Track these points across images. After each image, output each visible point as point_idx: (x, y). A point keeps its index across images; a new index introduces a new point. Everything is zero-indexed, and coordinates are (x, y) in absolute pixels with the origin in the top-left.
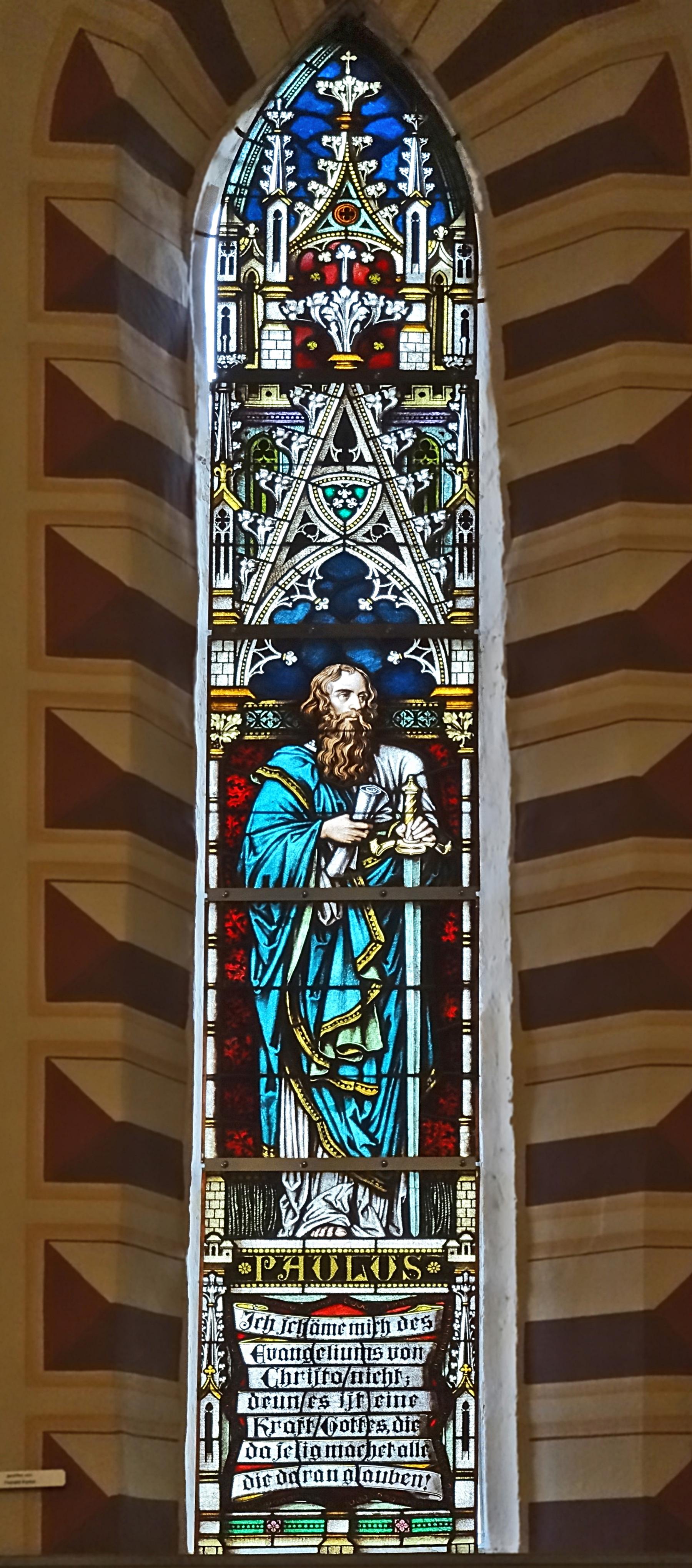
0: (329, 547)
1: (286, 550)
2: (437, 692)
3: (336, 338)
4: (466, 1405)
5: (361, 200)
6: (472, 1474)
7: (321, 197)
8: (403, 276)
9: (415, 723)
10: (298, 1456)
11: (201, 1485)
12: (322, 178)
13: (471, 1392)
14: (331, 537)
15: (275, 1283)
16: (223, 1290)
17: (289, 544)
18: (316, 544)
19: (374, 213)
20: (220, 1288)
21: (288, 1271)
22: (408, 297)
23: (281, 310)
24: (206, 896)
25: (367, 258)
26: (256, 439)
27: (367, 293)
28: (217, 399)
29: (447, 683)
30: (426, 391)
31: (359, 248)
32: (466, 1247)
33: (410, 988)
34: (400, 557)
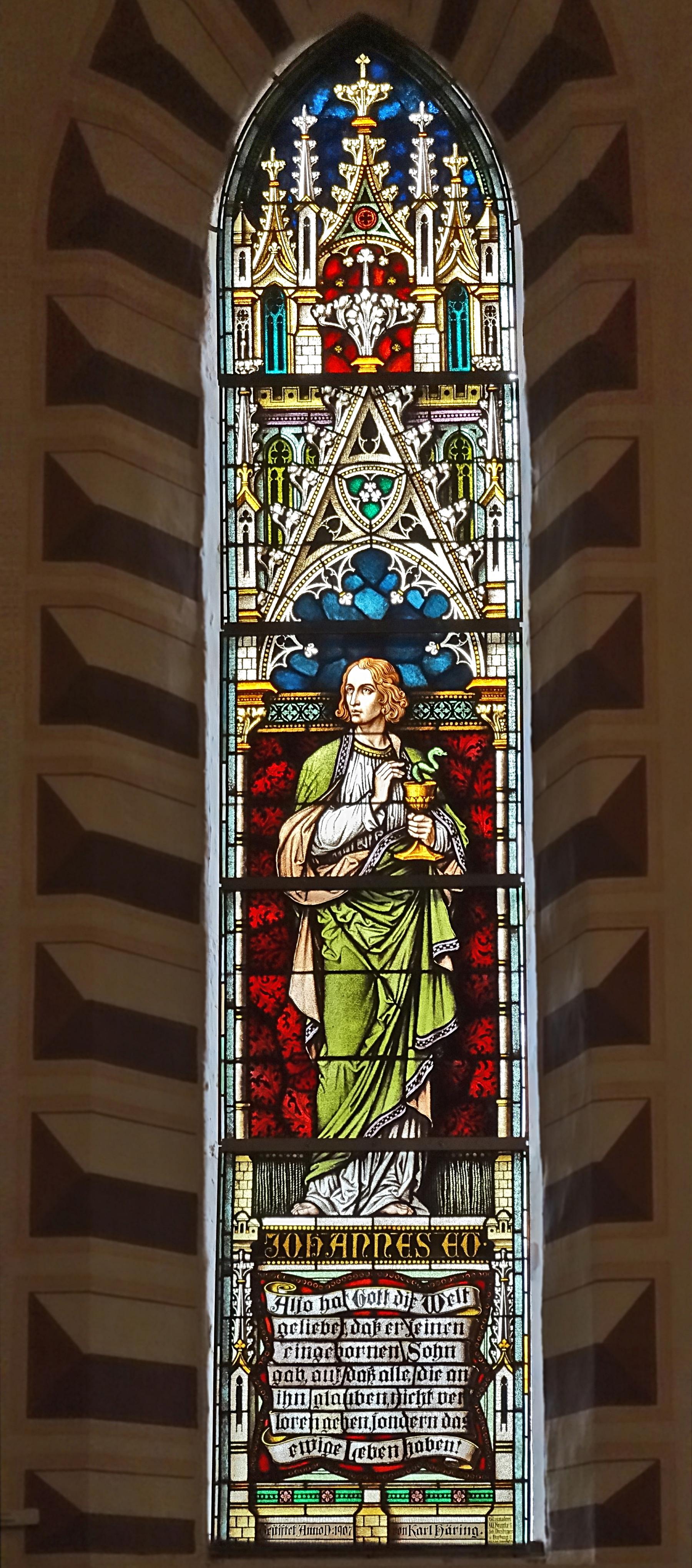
0: (348, 546)
1: (308, 548)
2: (474, 684)
3: (357, 340)
4: (504, 1380)
5: (377, 203)
6: (511, 1446)
7: (343, 202)
8: (415, 277)
9: (452, 715)
10: (311, 1427)
11: (232, 1455)
12: (343, 184)
13: (509, 1367)
14: (356, 532)
15: (326, 1261)
16: (251, 1266)
17: (309, 543)
18: (335, 542)
19: (389, 216)
20: (248, 1264)
21: (334, 1249)
22: (420, 299)
23: (312, 313)
24: (220, 885)
25: (384, 261)
26: (275, 440)
27: (384, 296)
28: (237, 401)
29: (483, 675)
30: (294, 392)
31: (377, 251)
32: (503, 1224)
33: (425, 972)
34: (433, 550)
